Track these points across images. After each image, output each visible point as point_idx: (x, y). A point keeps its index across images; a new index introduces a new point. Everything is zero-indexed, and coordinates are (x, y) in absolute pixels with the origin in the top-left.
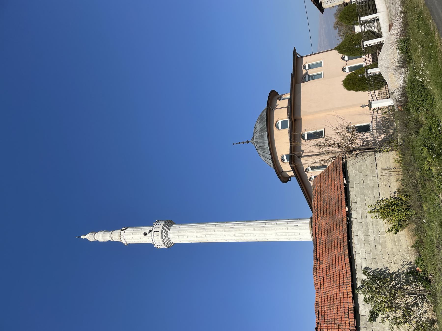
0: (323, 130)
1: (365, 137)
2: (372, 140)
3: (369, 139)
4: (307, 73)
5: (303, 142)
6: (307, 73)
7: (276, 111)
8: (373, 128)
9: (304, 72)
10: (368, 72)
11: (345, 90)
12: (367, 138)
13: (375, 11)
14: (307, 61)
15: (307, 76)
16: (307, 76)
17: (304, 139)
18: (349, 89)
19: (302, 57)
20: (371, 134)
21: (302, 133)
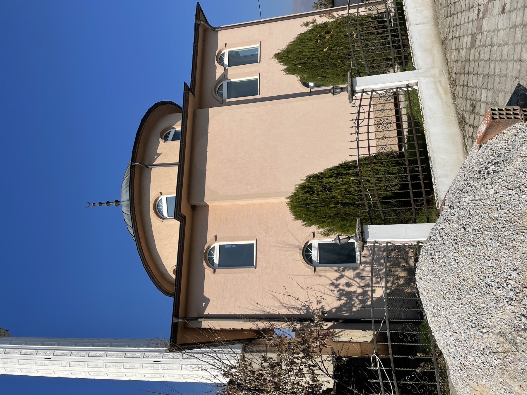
0: (254, 242)
1: (343, 281)
2: (360, 294)
3: (352, 289)
4: (224, 76)
5: (208, 271)
6: (224, 76)
7: (155, 171)
8: (363, 260)
9: (219, 71)
10: (357, 89)
11: (289, 215)
12: (348, 285)
13: (405, 62)
14: (228, 41)
15: (225, 84)
16: (225, 84)
17: (211, 263)
18: (298, 215)
19: (215, 30)
20: (358, 275)
21: (209, 247)
